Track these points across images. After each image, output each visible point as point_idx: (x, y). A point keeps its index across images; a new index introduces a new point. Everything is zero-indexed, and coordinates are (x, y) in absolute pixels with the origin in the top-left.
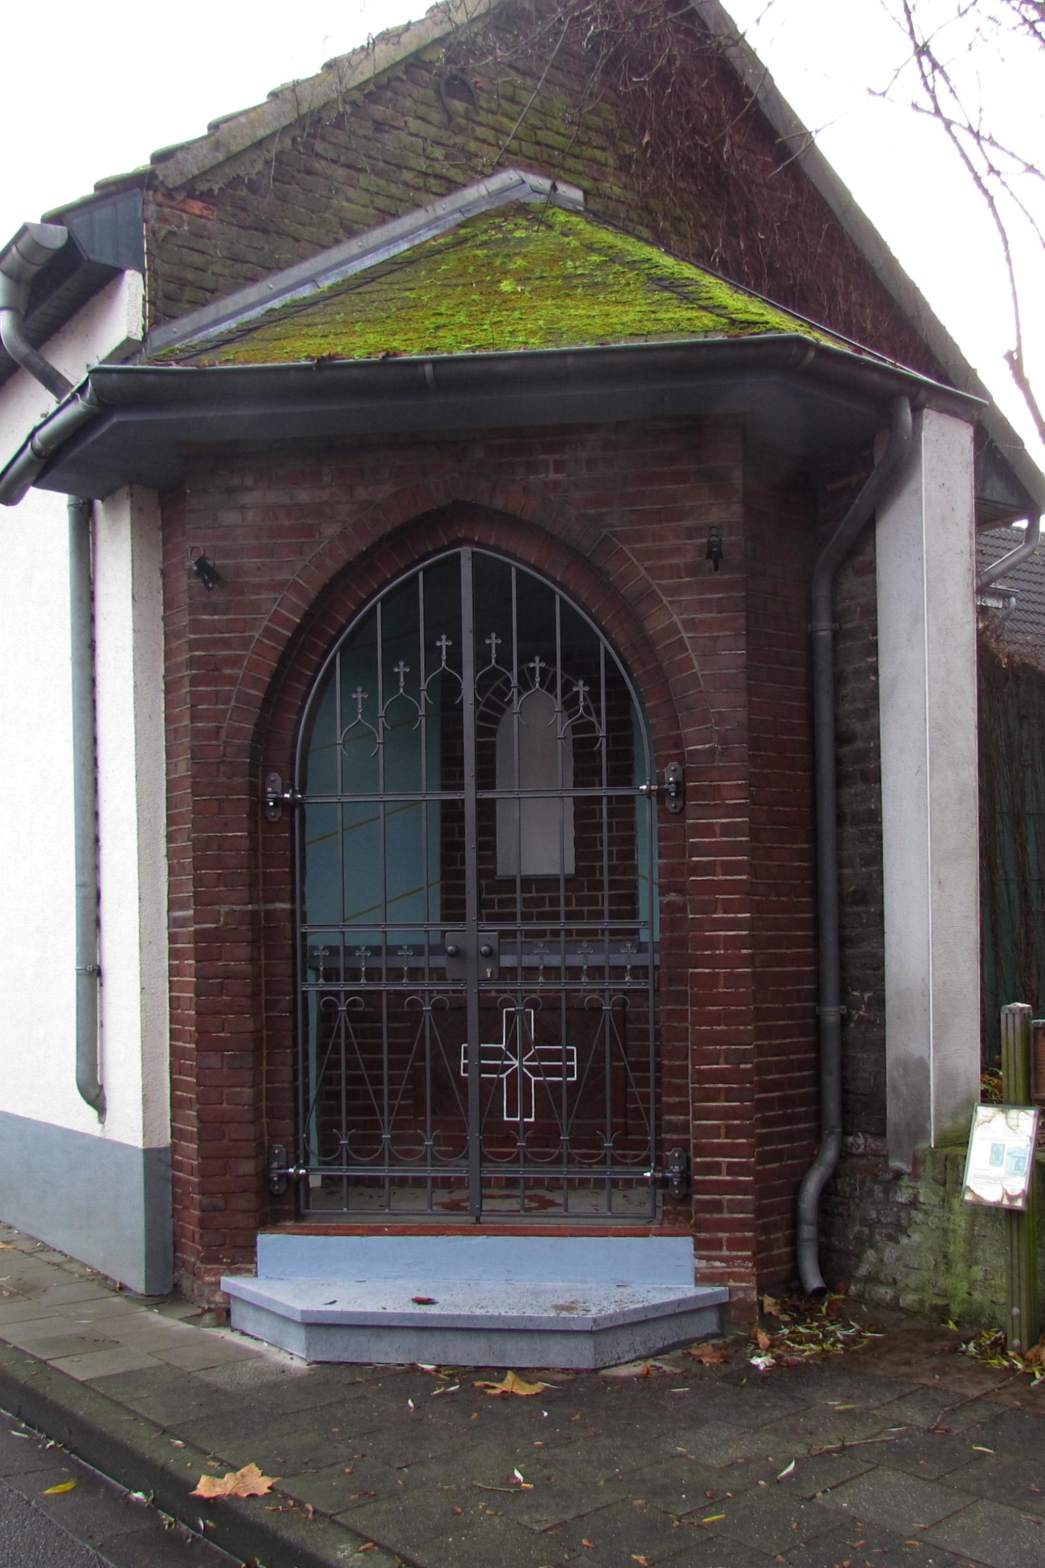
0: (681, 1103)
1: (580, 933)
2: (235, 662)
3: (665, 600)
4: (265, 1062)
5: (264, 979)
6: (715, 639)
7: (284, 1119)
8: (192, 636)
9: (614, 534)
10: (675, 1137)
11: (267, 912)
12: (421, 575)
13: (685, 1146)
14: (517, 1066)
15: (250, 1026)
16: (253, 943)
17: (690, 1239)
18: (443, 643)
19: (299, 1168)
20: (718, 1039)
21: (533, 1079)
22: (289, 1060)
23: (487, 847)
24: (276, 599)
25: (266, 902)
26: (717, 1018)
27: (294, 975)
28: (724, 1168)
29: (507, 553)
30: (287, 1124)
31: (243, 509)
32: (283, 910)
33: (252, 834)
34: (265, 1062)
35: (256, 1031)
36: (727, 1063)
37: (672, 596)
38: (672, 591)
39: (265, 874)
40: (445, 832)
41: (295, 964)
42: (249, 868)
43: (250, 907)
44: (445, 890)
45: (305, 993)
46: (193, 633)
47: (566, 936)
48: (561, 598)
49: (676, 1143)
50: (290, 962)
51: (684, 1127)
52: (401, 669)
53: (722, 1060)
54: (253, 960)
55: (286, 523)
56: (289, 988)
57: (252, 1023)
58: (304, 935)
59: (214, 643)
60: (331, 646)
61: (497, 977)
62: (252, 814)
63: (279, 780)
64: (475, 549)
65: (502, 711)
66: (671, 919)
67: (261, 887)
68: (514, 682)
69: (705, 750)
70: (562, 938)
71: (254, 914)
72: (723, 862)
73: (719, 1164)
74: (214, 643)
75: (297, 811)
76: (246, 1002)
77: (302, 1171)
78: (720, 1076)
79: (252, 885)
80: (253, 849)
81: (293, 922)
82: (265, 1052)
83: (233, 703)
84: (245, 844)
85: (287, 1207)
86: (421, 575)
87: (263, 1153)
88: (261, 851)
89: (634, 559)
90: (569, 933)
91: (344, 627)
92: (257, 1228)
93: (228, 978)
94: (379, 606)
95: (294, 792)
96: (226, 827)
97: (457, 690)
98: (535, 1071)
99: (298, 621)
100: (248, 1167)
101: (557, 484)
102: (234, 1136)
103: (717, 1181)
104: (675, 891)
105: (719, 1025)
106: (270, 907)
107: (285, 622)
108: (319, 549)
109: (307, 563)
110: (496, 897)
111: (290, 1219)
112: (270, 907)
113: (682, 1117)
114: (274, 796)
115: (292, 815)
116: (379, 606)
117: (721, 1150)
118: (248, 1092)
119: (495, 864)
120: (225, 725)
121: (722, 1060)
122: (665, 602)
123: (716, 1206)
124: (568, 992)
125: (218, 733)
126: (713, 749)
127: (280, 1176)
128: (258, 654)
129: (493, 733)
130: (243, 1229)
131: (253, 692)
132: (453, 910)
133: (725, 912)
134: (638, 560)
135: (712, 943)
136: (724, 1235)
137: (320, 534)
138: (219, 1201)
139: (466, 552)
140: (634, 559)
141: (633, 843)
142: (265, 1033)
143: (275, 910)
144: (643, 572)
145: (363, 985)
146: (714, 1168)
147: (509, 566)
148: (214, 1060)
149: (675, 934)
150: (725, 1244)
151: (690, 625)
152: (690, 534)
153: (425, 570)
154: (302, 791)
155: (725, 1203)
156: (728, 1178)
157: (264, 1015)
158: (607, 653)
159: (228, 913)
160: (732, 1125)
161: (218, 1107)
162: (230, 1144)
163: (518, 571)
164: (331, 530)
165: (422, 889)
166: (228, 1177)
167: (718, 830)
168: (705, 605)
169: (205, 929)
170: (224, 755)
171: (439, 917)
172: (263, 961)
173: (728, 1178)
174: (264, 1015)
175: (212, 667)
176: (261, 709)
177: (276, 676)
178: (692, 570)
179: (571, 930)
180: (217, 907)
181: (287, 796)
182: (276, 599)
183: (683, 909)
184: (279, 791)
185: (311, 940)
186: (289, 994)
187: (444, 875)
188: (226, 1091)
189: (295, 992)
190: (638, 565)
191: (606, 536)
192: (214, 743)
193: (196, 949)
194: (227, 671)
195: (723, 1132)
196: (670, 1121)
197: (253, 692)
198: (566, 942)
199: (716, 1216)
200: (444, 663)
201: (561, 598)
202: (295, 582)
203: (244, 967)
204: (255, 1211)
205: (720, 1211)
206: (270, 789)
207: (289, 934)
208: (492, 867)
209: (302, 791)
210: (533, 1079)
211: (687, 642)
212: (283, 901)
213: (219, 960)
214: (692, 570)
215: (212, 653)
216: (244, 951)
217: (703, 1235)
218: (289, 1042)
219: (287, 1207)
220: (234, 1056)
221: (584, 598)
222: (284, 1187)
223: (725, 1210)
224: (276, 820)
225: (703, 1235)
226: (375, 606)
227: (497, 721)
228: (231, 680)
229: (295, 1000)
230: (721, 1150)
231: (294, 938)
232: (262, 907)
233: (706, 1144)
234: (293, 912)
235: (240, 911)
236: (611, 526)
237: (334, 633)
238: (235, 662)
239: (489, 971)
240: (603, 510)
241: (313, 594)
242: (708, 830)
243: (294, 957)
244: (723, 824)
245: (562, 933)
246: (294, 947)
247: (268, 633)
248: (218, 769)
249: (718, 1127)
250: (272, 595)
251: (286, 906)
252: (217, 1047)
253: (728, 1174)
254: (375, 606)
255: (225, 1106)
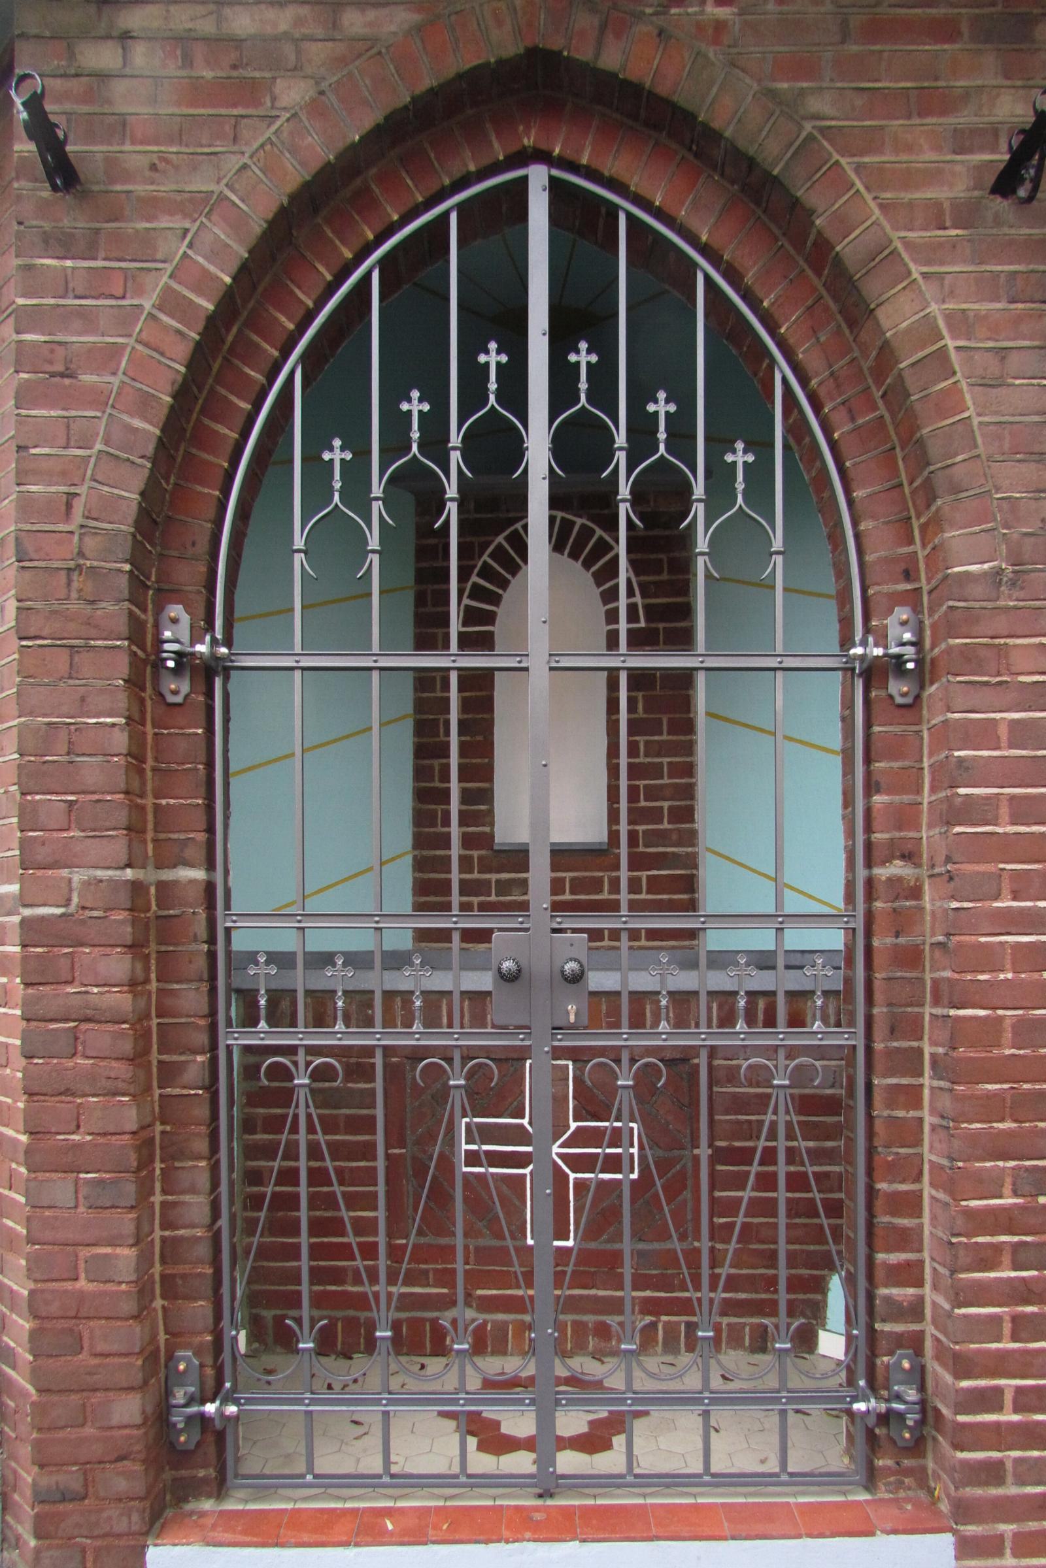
0: (908, 1264)
1: (653, 934)
2: (108, 357)
3: (916, 271)
4: (158, 1186)
5: (155, 1021)
6: (1002, 353)
7: (195, 1299)
8: (21, 301)
9: (822, 130)
10: (899, 1328)
11: (162, 886)
12: (454, 217)
13: (915, 1343)
14: (544, 1157)
15: (131, 1118)
16: (135, 947)
17: (948, 1539)
18: (493, 357)
19: (225, 1402)
20: (1001, 1149)
21: (572, 1176)
22: (204, 1181)
23: (480, 797)
24: (186, 231)
25: (159, 866)
26: (992, 1108)
27: (213, 1013)
28: (1008, 1398)
29: (612, 184)
30: (201, 1307)
31: (126, 37)
32: (192, 882)
33: (134, 722)
34: (158, 1186)
35: (143, 1128)
36: (1015, 1194)
37: (928, 263)
38: (929, 253)
39: (157, 807)
40: (420, 773)
41: (213, 990)
42: (127, 793)
43: (129, 873)
44: (420, 865)
45: (229, 1048)
46: (23, 296)
47: (630, 940)
48: (708, 279)
49: (899, 1341)
50: (205, 987)
51: (915, 1310)
52: (415, 406)
53: (1007, 1189)
54: (134, 985)
55: (208, 74)
56: (203, 1039)
57: (133, 1112)
58: (228, 931)
59: (65, 317)
60: (286, 354)
61: (585, 1020)
62: (134, 683)
63: (185, 619)
64: (555, 173)
65: (514, 569)
66: (894, 910)
67: (150, 835)
68: (621, 439)
69: (985, 574)
70: (625, 942)
71: (137, 887)
72: (1012, 798)
73: (999, 1391)
74: (65, 317)
75: (218, 683)
76: (121, 1069)
77: (232, 1409)
78: (1004, 1221)
79: (134, 830)
80: (136, 756)
81: (211, 906)
82: (158, 1166)
83: (99, 446)
84: (120, 741)
85: (201, 1473)
86: (454, 217)
87: (157, 1366)
88: (150, 762)
89: (859, 185)
90: (634, 934)
91: (310, 316)
92: (146, 1534)
93: (88, 1020)
94: (376, 276)
95: (214, 642)
96: (83, 705)
97: (515, 450)
98: (577, 1163)
99: (228, 280)
100: (128, 1409)
101: (720, 26)
102: (101, 1347)
103: (998, 1424)
104: (903, 857)
105: (1002, 1120)
106: (168, 875)
107: (203, 281)
108: (269, 133)
109: (246, 159)
110: (494, 877)
111: (209, 1496)
112: (168, 875)
113: (911, 1291)
114: (175, 647)
115: (210, 694)
116: (376, 276)
117: (1000, 1365)
118: (127, 1253)
119: (492, 824)
120: (82, 490)
121: (1007, 1189)
122: (915, 275)
123: (993, 1473)
124: (713, 1051)
125: (69, 506)
126: (999, 572)
127: (190, 1419)
128: (146, 345)
129: (490, 618)
130: (119, 1536)
131: (138, 423)
132: (430, 892)
133: (1014, 899)
134: (867, 188)
135: (989, 959)
136: (1007, 1528)
137: (274, 99)
138: (70, 1478)
139: (538, 176)
140: (859, 185)
141: (692, 797)
142: (159, 1128)
143: (175, 883)
144: (877, 212)
145: (339, 1035)
146: (989, 1400)
147: (613, 210)
148: (61, 1189)
149: (901, 940)
150: (1008, 1544)
151: (960, 323)
152: (963, 141)
153: (460, 207)
154: (228, 642)
155: (1009, 1465)
156: (1016, 1418)
157: (157, 1092)
158: (785, 381)
159: (87, 884)
160: (1025, 1316)
161: (68, 1285)
162: (97, 1361)
163: (630, 217)
164: (292, 93)
165: (371, 869)
166: (89, 1430)
167: (1003, 732)
168: (989, 287)
169: (43, 919)
170: (81, 554)
171: (410, 905)
172: (154, 986)
173: (1016, 1418)
174: (157, 1092)
175: (60, 367)
176: (155, 461)
177: (184, 394)
178: (966, 215)
179: (601, 930)
180: (65, 872)
181: (201, 648)
182: (186, 231)
183: (915, 892)
184: (186, 638)
185: (240, 943)
186: (203, 1053)
187: (420, 841)
188: (84, 1253)
189: (214, 1047)
190: (868, 197)
191: (810, 138)
192: (61, 527)
193: (25, 959)
194: (88, 378)
195: (1007, 1328)
196: (888, 1299)
197: (138, 423)
198: (631, 948)
199: (994, 1491)
200: (492, 398)
201: (708, 279)
202: (222, 198)
203: (120, 1000)
204: (141, 1499)
205: (1000, 1481)
206: (168, 634)
207: (201, 928)
208: (487, 829)
209: (228, 642)
210: (572, 1176)
211: (953, 355)
212: (191, 865)
213: (70, 982)
214: (966, 215)
215: (59, 338)
216: (118, 965)
217: (971, 1529)
218: (202, 1146)
219: (201, 1473)
220: (101, 1182)
221: (749, 279)
222: (196, 1436)
223: (1010, 1479)
224: (179, 699)
225: (971, 1529)
226: (367, 277)
227: (496, 600)
228: (98, 398)
229: (214, 1062)
230: (1000, 1365)
231: (212, 940)
232: (149, 875)
233: (979, 1351)
234: (210, 887)
235: (110, 880)
236: (817, 117)
237: (291, 326)
238: (108, 357)
239: (572, 1008)
240: (805, 85)
241: (257, 227)
242: (985, 734)
243: (213, 978)
244: (1013, 720)
245: (456, 937)
246: (212, 956)
247: (170, 302)
248: (69, 582)
249: (996, 1319)
250: (179, 223)
251: (199, 874)
252: (68, 1163)
253: (1016, 1410)
254: (367, 277)
255: (82, 1284)
